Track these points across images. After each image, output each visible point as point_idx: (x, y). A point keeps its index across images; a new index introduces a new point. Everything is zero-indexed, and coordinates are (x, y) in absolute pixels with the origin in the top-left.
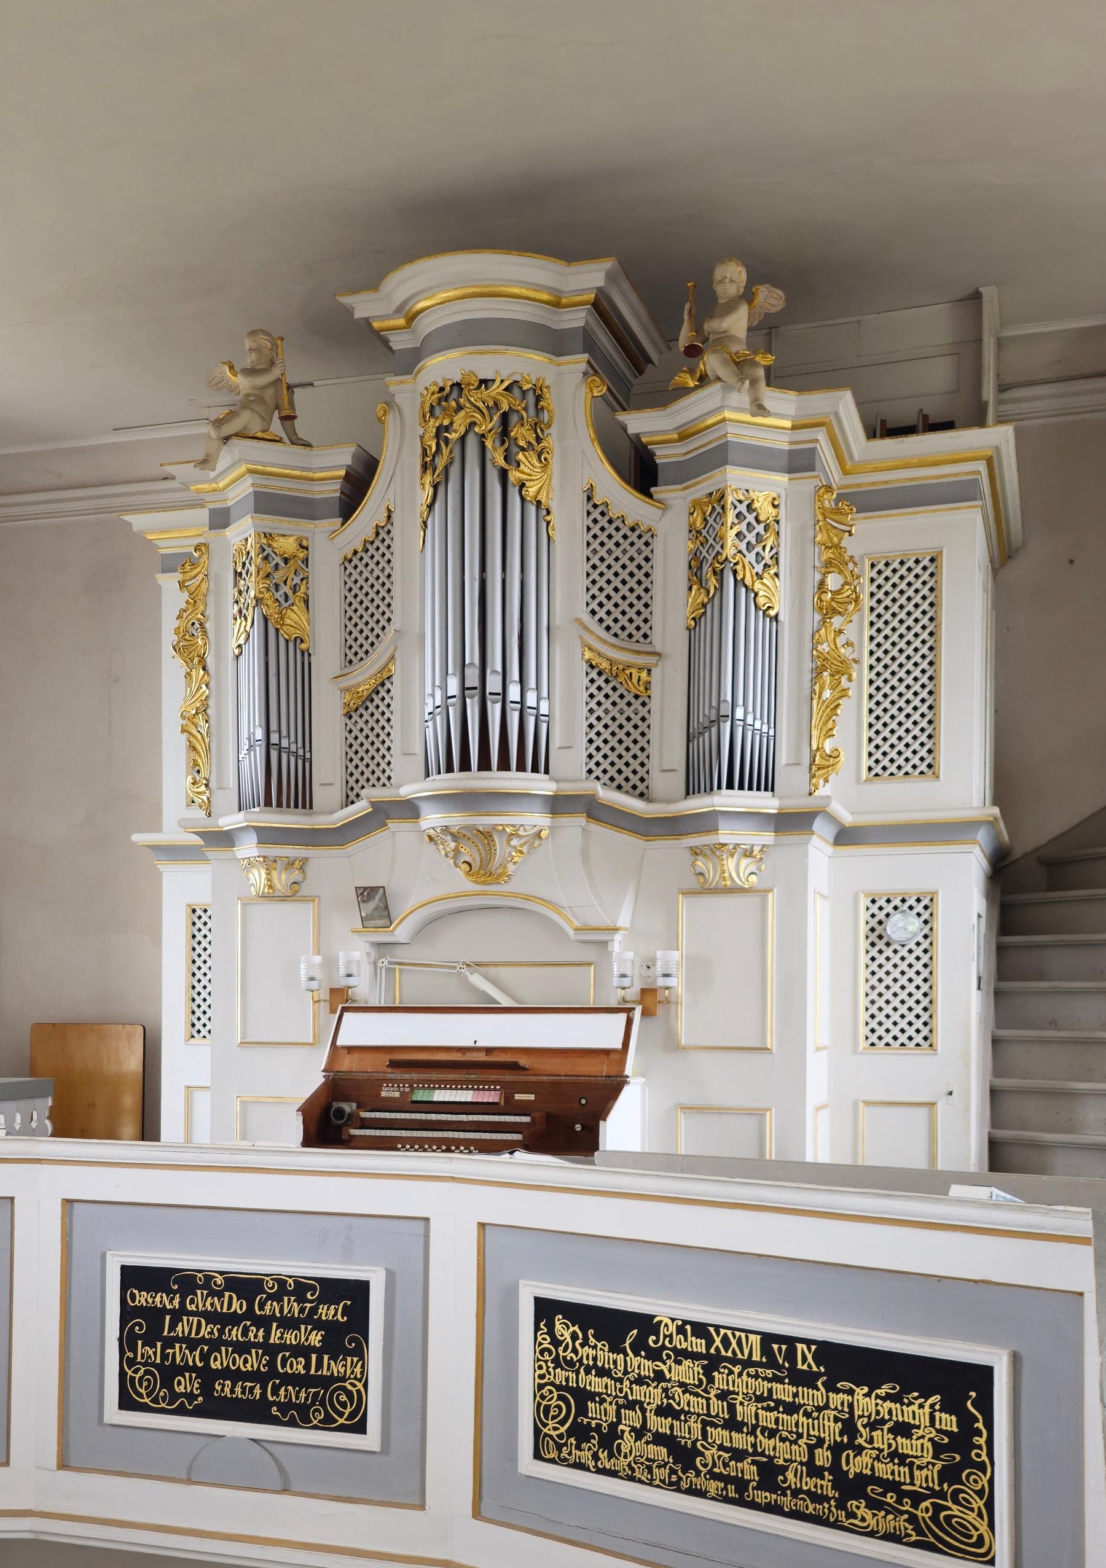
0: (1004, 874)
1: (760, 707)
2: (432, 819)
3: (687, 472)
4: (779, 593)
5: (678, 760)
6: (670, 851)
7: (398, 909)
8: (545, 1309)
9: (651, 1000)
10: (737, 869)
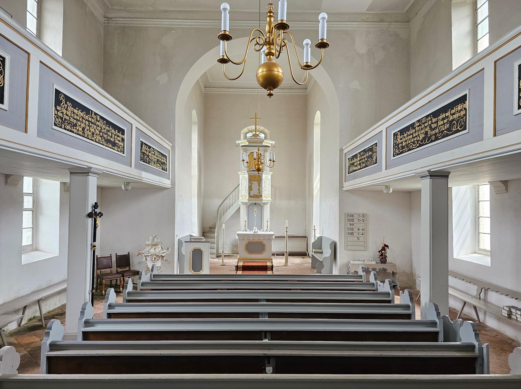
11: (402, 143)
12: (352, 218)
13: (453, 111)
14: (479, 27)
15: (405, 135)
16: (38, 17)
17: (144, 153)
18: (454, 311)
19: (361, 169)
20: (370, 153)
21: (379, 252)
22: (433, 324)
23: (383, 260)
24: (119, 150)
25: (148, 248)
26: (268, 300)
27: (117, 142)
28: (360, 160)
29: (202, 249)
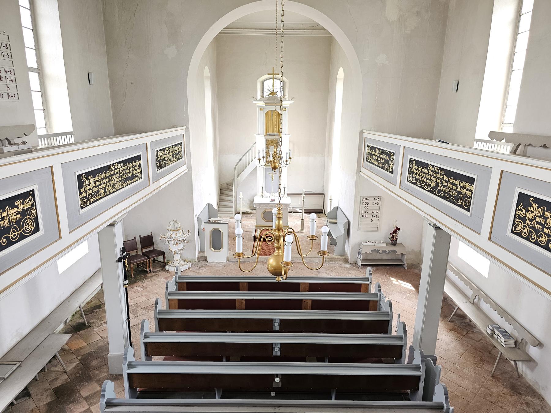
12: (367, 201)
13: (462, 184)
14: (519, 36)
15: (420, 169)
16: (31, 6)
18: (451, 303)
19: (377, 166)
21: (391, 234)
22: (417, 368)
23: (394, 242)
25: (169, 233)
29: (221, 230)
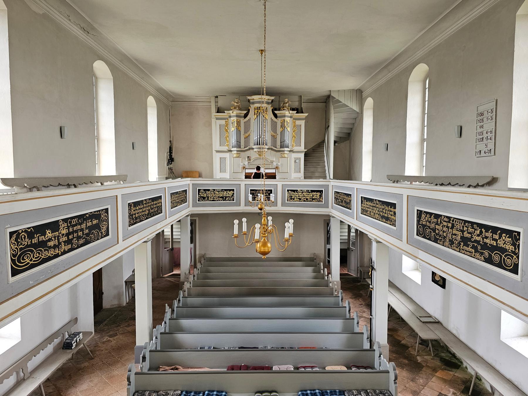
0: (306, 155)
1: (288, 140)
2: (255, 150)
3: (281, 117)
4: (289, 129)
5: (279, 144)
6: (279, 153)
7: (252, 159)
8: (288, 190)
9: (277, 168)
10: (286, 155)
11: (135, 214)
15: (138, 208)
17: (424, 226)
20: (95, 222)
24: (391, 223)
26: (255, 349)
27: (390, 216)
28: (68, 235)
